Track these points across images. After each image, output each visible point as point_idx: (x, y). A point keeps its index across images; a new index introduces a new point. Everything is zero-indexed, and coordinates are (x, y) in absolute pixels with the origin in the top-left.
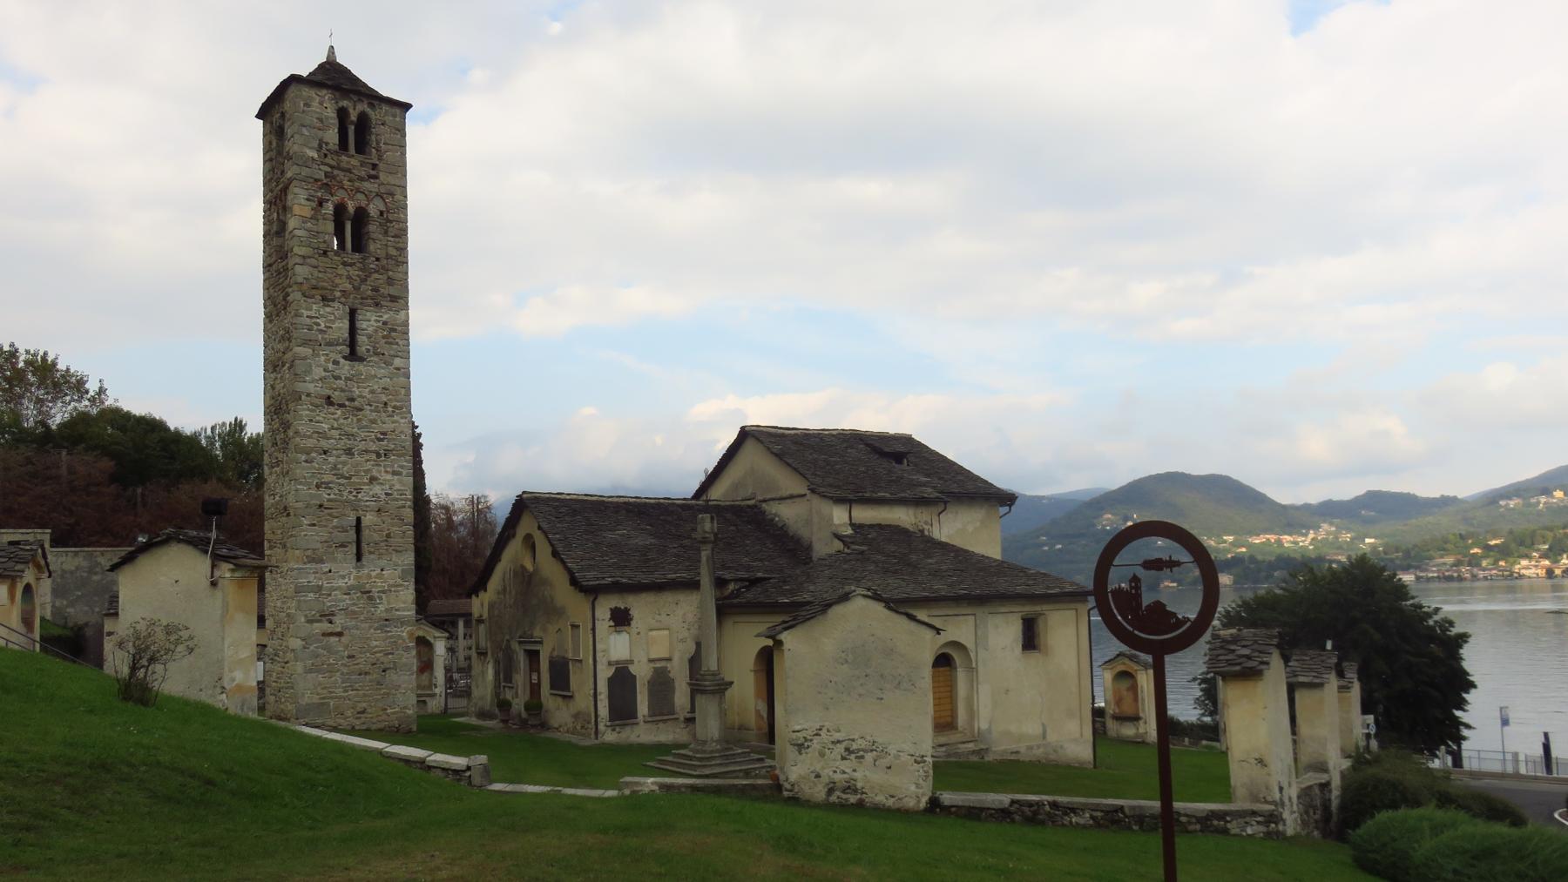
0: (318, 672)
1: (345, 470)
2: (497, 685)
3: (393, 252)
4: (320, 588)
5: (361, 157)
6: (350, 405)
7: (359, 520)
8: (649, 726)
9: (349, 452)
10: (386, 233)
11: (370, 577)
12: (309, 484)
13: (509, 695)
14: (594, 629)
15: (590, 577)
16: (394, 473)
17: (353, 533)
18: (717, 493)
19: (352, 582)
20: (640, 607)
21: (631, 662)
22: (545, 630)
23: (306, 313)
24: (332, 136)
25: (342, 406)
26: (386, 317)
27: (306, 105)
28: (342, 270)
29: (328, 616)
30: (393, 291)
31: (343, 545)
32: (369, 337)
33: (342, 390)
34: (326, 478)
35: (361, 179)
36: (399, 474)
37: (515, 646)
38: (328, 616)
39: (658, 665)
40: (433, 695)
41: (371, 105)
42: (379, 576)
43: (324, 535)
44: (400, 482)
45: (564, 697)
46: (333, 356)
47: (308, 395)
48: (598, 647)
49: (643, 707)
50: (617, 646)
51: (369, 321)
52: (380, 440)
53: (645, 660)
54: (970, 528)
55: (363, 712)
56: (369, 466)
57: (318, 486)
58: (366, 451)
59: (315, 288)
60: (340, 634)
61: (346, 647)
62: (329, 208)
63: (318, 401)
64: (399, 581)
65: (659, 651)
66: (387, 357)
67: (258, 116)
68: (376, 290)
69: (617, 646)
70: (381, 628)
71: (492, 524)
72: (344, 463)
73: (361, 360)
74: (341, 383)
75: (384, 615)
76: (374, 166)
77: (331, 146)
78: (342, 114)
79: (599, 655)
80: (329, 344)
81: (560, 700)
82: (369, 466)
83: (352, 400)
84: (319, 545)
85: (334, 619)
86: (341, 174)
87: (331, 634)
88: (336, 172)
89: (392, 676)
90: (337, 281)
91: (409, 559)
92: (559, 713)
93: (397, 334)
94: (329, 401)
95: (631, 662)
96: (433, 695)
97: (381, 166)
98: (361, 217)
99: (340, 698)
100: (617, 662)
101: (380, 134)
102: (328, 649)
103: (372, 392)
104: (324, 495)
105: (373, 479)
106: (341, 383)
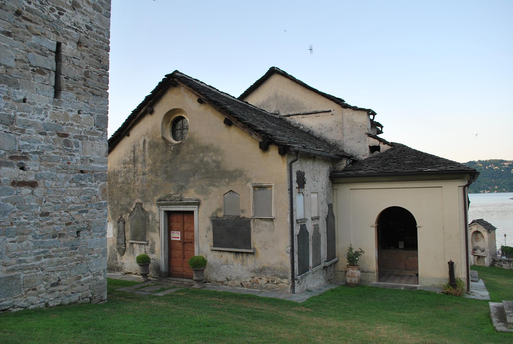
11: (66, 116)
19: (48, 120)
38: (20, 159)
42: (76, 119)
54: (63, 76)
60: (33, 185)
61: (40, 201)
64: (95, 129)
67: (383, 133)
71: (470, 193)
85: (29, 164)
87: (23, 184)
99: (33, 267)
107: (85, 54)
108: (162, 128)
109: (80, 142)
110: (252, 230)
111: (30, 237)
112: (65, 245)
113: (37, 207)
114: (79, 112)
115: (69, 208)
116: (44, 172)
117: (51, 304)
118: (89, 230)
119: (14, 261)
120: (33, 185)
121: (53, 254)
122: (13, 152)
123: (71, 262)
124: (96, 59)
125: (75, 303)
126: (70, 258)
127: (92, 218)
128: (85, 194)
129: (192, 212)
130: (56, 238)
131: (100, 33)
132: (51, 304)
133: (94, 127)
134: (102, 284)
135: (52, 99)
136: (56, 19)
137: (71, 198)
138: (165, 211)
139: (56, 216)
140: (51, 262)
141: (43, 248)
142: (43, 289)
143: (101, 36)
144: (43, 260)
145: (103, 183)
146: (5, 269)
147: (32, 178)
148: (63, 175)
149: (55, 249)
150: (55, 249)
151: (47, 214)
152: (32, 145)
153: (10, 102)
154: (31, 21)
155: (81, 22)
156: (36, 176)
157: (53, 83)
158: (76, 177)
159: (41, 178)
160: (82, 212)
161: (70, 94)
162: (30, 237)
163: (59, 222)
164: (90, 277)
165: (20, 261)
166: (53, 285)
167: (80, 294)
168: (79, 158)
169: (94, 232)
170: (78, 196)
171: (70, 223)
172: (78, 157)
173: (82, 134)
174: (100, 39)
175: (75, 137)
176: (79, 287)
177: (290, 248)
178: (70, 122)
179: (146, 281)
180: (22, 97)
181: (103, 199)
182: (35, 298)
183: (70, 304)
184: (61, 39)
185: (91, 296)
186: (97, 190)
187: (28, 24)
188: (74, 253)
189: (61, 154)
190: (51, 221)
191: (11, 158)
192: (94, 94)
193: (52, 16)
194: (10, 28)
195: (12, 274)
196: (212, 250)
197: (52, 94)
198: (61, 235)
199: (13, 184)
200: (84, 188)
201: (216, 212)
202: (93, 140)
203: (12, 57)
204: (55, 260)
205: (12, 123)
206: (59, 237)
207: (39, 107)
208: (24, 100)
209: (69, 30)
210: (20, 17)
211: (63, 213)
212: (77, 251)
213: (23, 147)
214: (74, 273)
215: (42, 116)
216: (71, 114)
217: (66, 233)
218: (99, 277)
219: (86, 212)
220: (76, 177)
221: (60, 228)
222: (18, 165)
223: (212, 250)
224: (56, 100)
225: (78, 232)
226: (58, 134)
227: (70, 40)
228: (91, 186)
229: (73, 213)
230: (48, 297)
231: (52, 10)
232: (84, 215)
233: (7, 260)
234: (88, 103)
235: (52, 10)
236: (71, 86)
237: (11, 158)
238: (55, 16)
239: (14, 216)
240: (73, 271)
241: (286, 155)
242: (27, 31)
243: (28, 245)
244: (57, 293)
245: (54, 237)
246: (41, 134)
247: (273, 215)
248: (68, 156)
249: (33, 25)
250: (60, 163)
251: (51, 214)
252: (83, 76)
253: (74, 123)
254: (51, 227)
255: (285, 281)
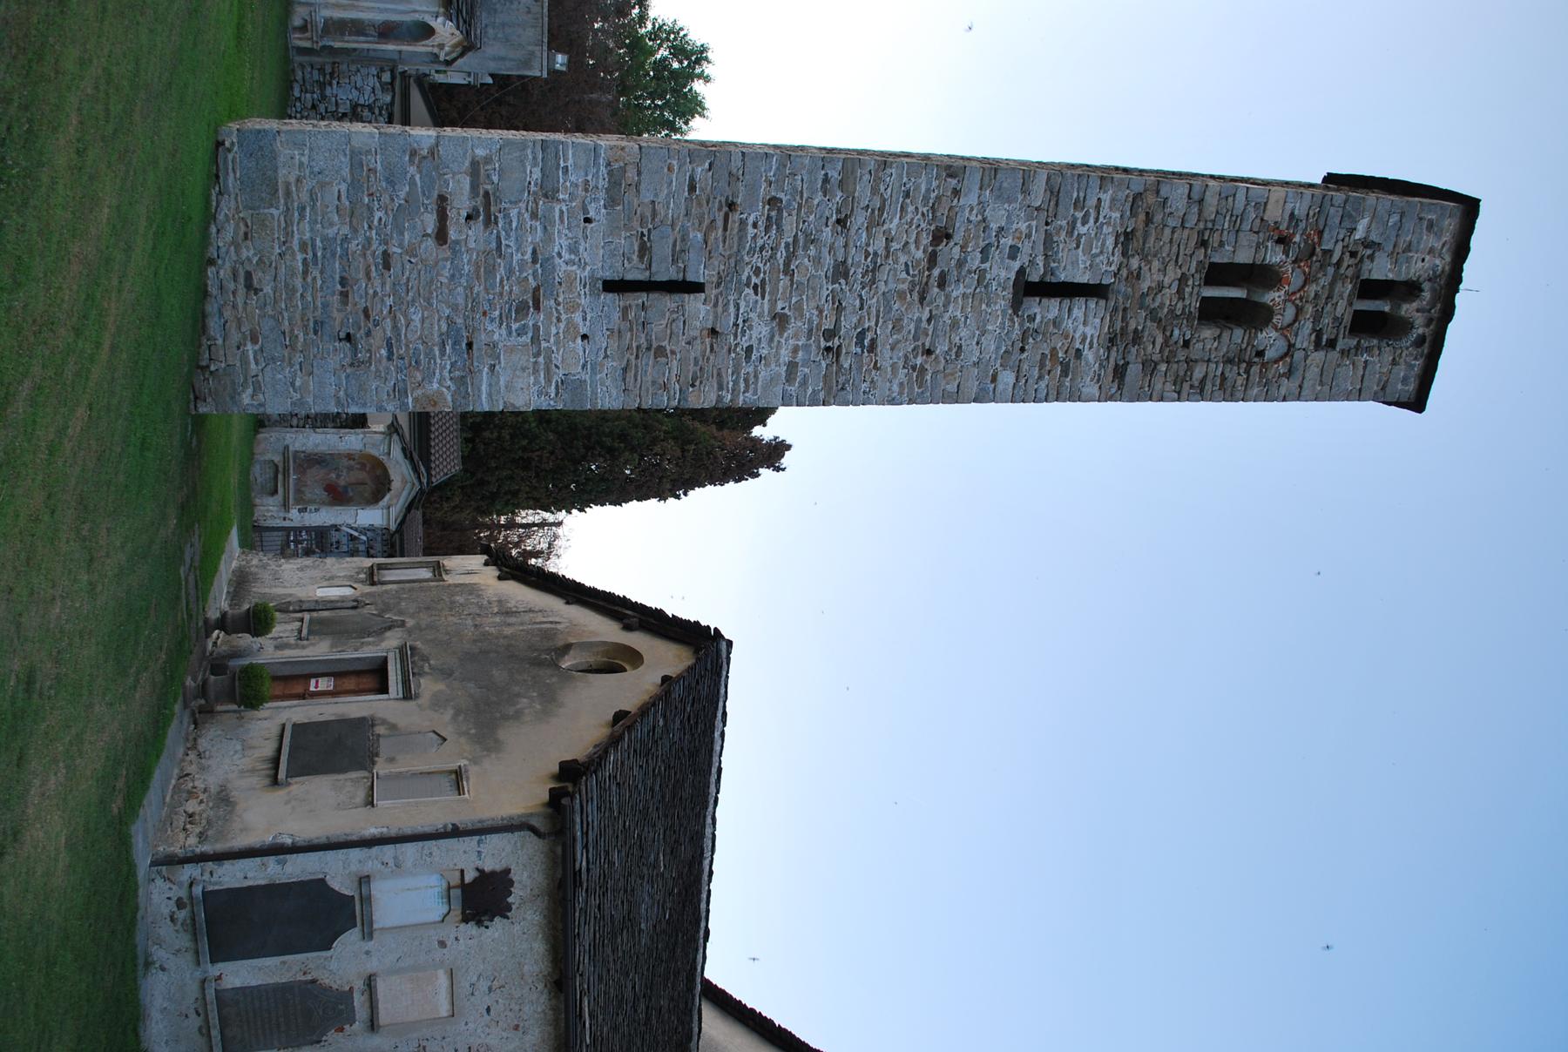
0: (354, 185)
1: (803, 261)
2: (302, 607)
3: (1198, 373)
4: (549, 193)
5: (1348, 319)
6: (931, 279)
7: (697, 288)
8: (193, 989)
9: (841, 271)
10: (1229, 361)
11: (573, 307)
12: (779, 182)
13: (283, 629)
14: (456, 832)
15: (587, 814)
16: (792, 367)
17: (672, 274)
18: (712, 1024)
19: (562, 268)
20: (518, 940)
21: (368, 934)
22: (437, 703)
23: (1106, 198)
24: (1381, 269)
25: (932, 259)
26: (1089, 355)
27: (1431, 226)
28: (1173, 274)
29: (485, 211)
30: (1134, 370)
31: (644, 250)
32: (1056, 323)
33: (961, 263)
34: (790, 224)
35: (1317, 317)
36: (790, 378)
37: (392, 641)
39: (359, 1001)
40: (285, 506)
41: (1420, 341)
43: (672, 209)
44: (773, 380)
45: (276, 761)
46: (1026, 248)
47: (956, 193)
48: (410, 849)
49: (241, 974)
50: (410, 896)
51: (1085, 323)
52: (860, 342)
53: (372, 965)
55: (249, 286)
56: (809, 311)
57: (773, 202)
58: (839, 309)
59: (1149, 219)
60: (441, 236)
61: (411, 251)
62: (1275, 256)
63: (943, 210)
64: (558, 376)
65: (395, 1001)
66: (1016, 356)
68: (1137, 338)
69: (410, 896)
70: (452, 332)
72: (817, 261)
73: (1016, 305)
74: (974, 261)
75: (481, 339)
76: (1332, 344)
77: (1367, 265)
78: (1411, 289)
79: (388, 851)
80: (1049, 241)
81: (268, 750)
82: (809, 311)
83: (942, 284)
84: (647, 197)
86: (1324, 281)
87: (442, 217)
88: (1331, 270)
89: (338, 355)
90: (1156, 264)
91: (608, 396)
92: (235, 753)
93: (1056, 380)
94: (942, 236)
95: (368, 934)
96: (285, 506)
97: (1334, 355)
98: (1252, 315)
99: (289, 234)
100: (367, 900)
101: (1379, 359)
102: (409, 208)
103: (955, 325)
104: (756, 214)
105: (781, 320)
106: (974, 261)
107: (698, 345)
108: (591, 644)
109: (526, 339)
110: (341, 777)
111: (346, 230)
112: (325, 306)
113: (401, 246)
114: (584, 337)
115: (399, 315)
116: (465, 258)
117: (211, 271)
118: (352, 365)
119: (305, 197)
120: (441, 236)
121: (309, 279)
122: (499, 200)
123: (290, 320)
124: (695, 373)
125: (204, 328)
126: (298, 316)
127: (378, 370)
128: (426, 355)
129: (384, 689)
130: (339, 287)
131: (746, 380)
132: (211, 271)
133: (561, 372)
134: (232, 398)
135: (600, 274)
136: (744, 278)
137: (417, 318)
138: (385, 659)
139: (383, 284)
140: (293, 275)
141: (324, 257)
142: (245, 254)
143: (742, 385)
144: (300, 257)
145: (449, 398)
146: (292, 179)
147: (452, 234)
148: (461, 300)
149: (319, 282)
150: (319, 282)
151: (387, 266)
152: (513, 234)
153: (580, 192)
154: (725, 229)
155: (755, 334)
156: (457, 242)
157: (629, 277)
158: (458, 330)
159: (455, 252)
160: (390, 346)
161: (616, 316)
162: (346, 230)
163: (371, 292)
164: (253, 366)
165: (304, 208)
166: (248, 275)
167: (220, 342)
168: (496, 337)
169: (347, 377)
170: (420, 338)
171: (367, 316)
172: (499, 334)
173: (544, 344)
174: (736, 383)
175: (536, 328)
176: (235, 337)
177: (289, 841)
178: (564, 317)
179: (206, 621)
180: (591, 214)
181: (416, 400)
182: (229, 238)
183: (204, 316)
184: (712, 292)
185: (212, 368)
186: (435, 386)
187: (720, 223)
188: (306, 327)
189: (501, 294)
190: (374, 274)
191: (487, 194)
192: (625, 370)
193: (747, 271)
194: (702, 190)
195: (281, 193)
196: (283, 726)
197: (608, 275)
198: (344, 295)
199: (442, 199)
200: (436, 349)
201: (384, 722)
202: (536, 371)
203: (656, 195)
204: (298, 282)
205: (546, 196)
206: (341, 293)
207: (581, 249)
208: (587, 220)
209: (732, 309)
210: (725, 209)
211: (389, 301)
212: (312, 335)
213: (507, 216)
214: (267, 325)
215: (566, 256)
216: (577, 317)
217: (349, 308)
218: (250, 391)
219: (390, 358)
220: (458, 330)
221: (358, 300)
222: (476, 209)
223: (283, 726)
224: (600, 285)
225: (348, 337)
226: (537, 289)
227: (716, 313)
228: (442, 368)
229: (388, 323)
230: (228, 265)
231: (757, 271)
232: (384, 352)
233: (308, 184)
234: (606, 356)
235: (757, 271)
236: (631, 316)
237: (487, 194)
238: (749, 278)
239: (385, 199)
240: (271, 323)
241: (550, 810)
242: (707, 222)
243: (332, 225)
244: (232, 286)
245: (343, 281)
246: (534, 252)
247: (380, 803)
248: (497, 313)
249: (720, 231)
250: (483, 294)
251: (386, 273)
252: (655, 345)
253: (562, 325)
254: (361, 275)
255: (192, 840)
